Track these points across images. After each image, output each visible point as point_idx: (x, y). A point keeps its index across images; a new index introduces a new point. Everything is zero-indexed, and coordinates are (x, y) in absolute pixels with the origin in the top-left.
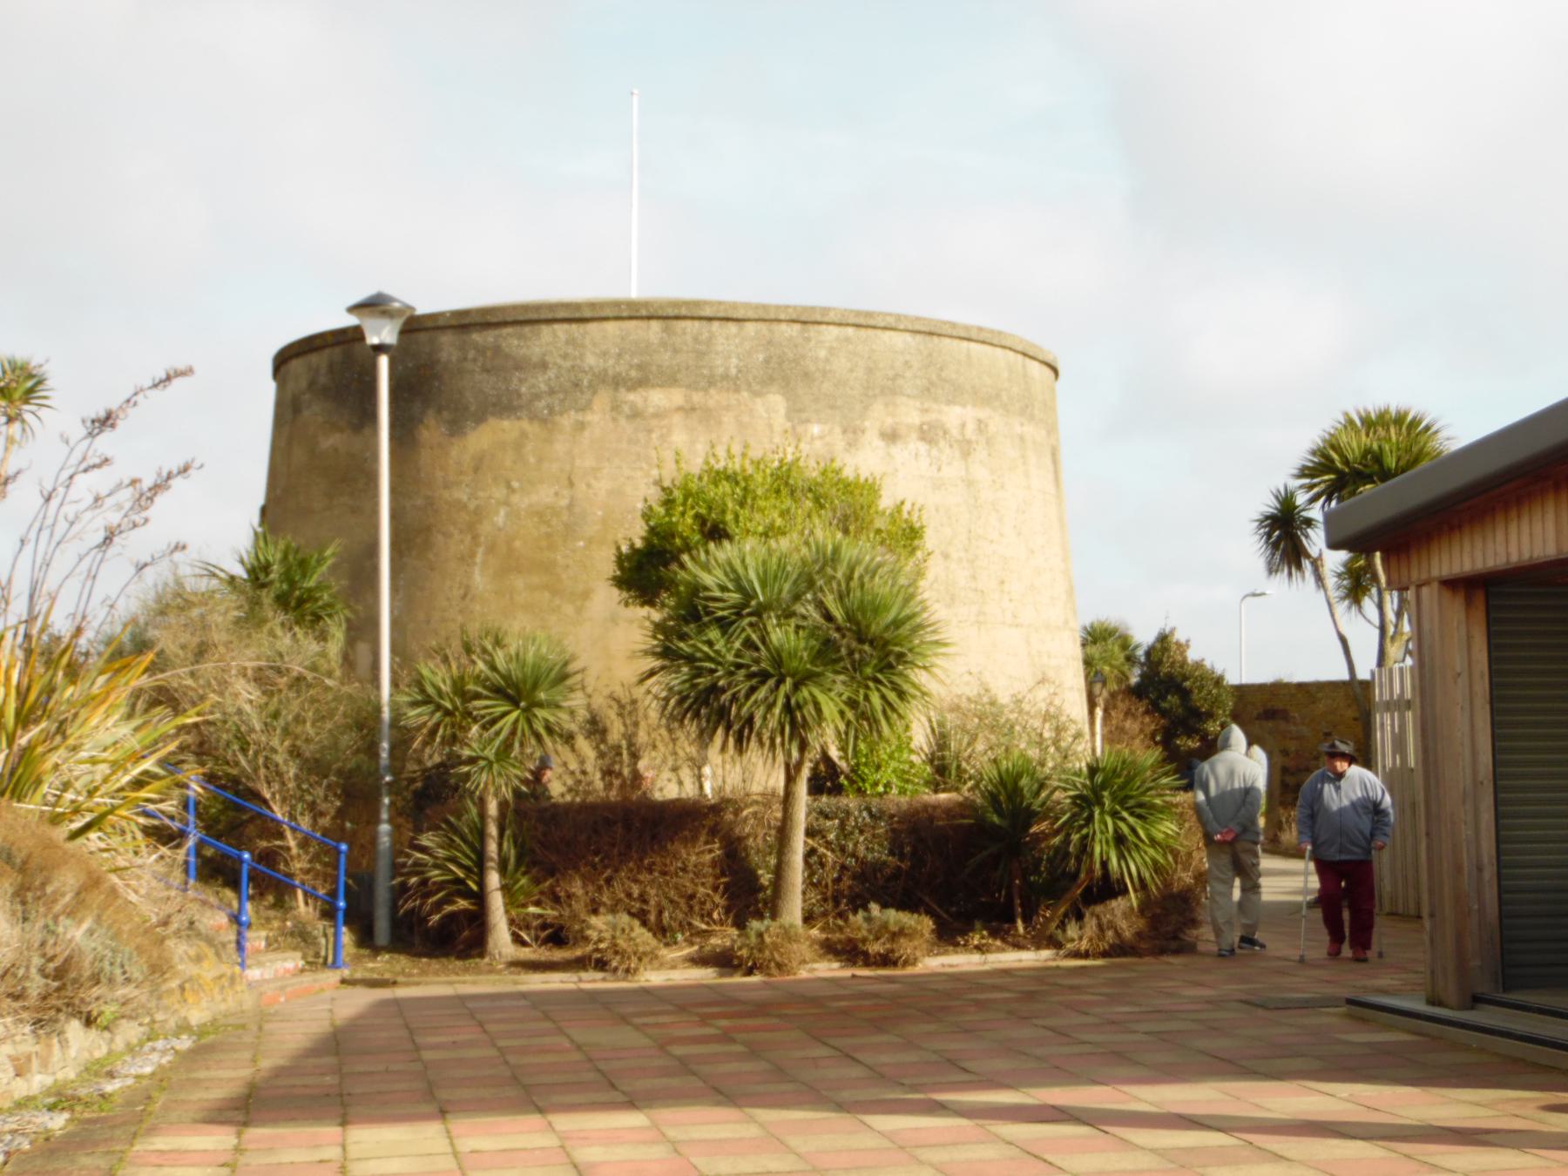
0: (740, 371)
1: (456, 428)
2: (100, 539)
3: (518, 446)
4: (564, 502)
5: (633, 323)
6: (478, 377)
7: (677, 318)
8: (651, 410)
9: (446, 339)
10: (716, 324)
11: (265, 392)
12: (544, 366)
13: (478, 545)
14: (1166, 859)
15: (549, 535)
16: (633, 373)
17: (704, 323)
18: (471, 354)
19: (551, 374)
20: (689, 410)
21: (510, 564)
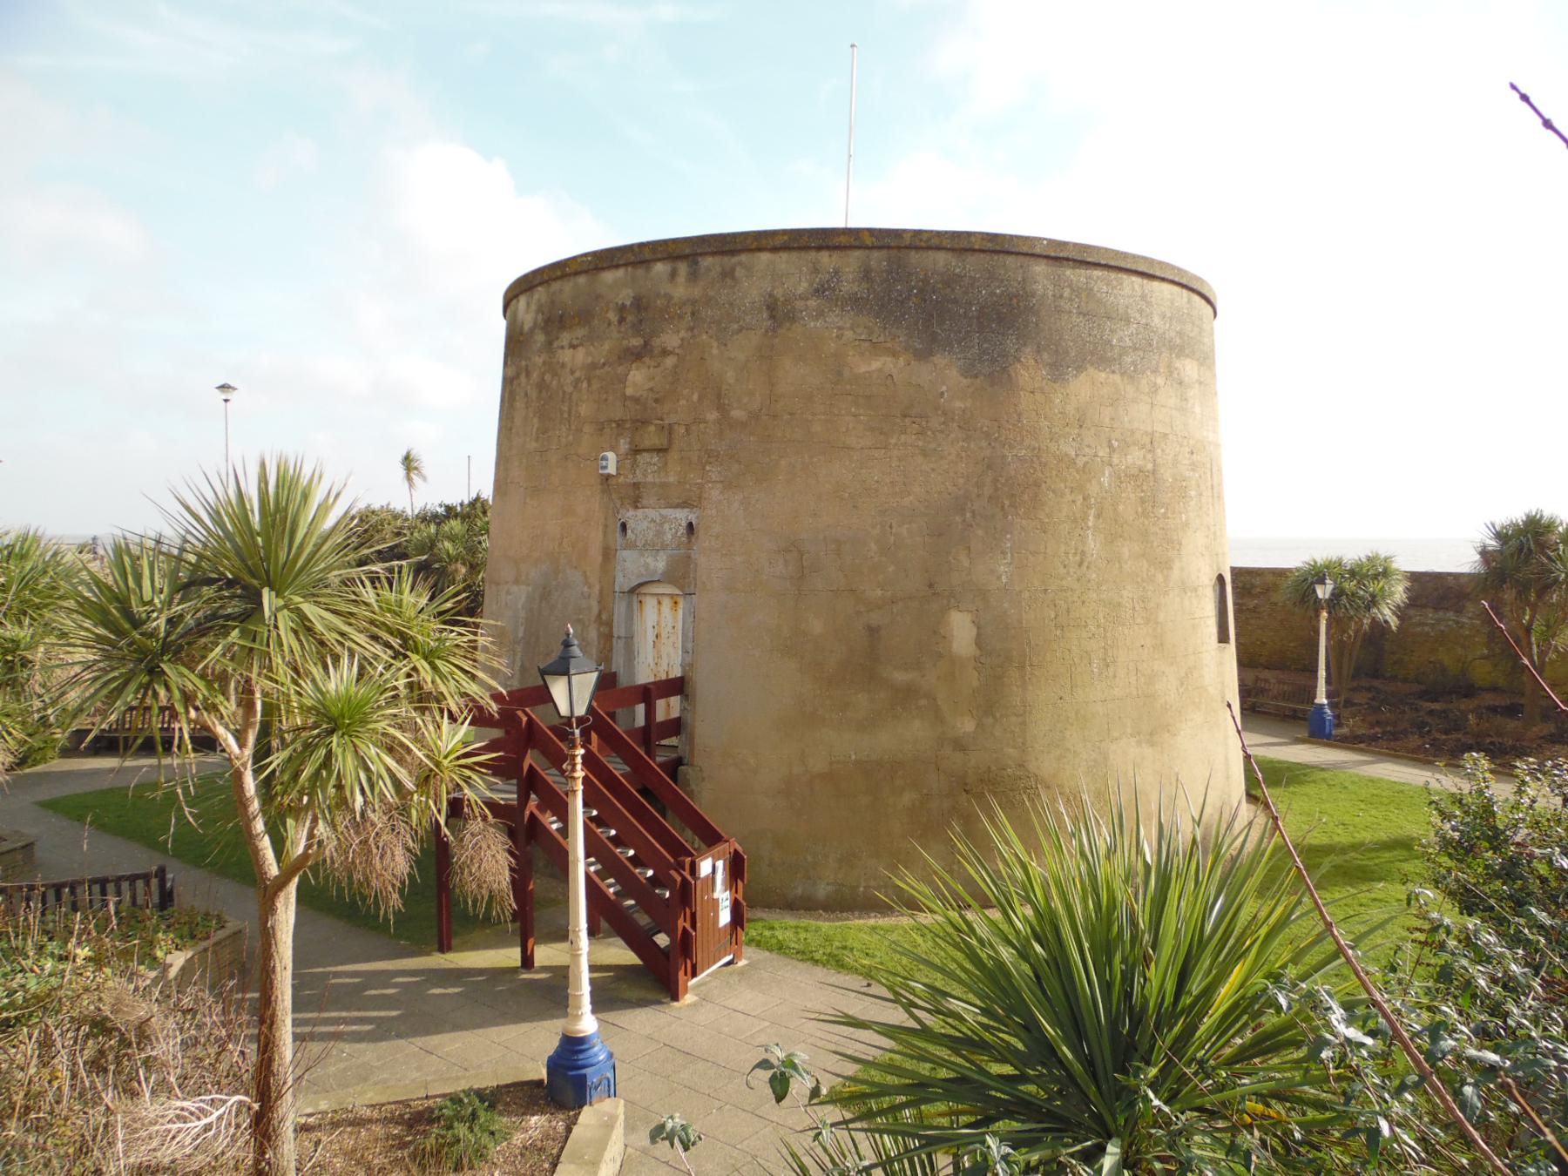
1: (1059, 369)
6: (1076, 319)
9: (1040, 269)
12: (1128, 321)
14: (1037, 1070)
19: (1133, 328)
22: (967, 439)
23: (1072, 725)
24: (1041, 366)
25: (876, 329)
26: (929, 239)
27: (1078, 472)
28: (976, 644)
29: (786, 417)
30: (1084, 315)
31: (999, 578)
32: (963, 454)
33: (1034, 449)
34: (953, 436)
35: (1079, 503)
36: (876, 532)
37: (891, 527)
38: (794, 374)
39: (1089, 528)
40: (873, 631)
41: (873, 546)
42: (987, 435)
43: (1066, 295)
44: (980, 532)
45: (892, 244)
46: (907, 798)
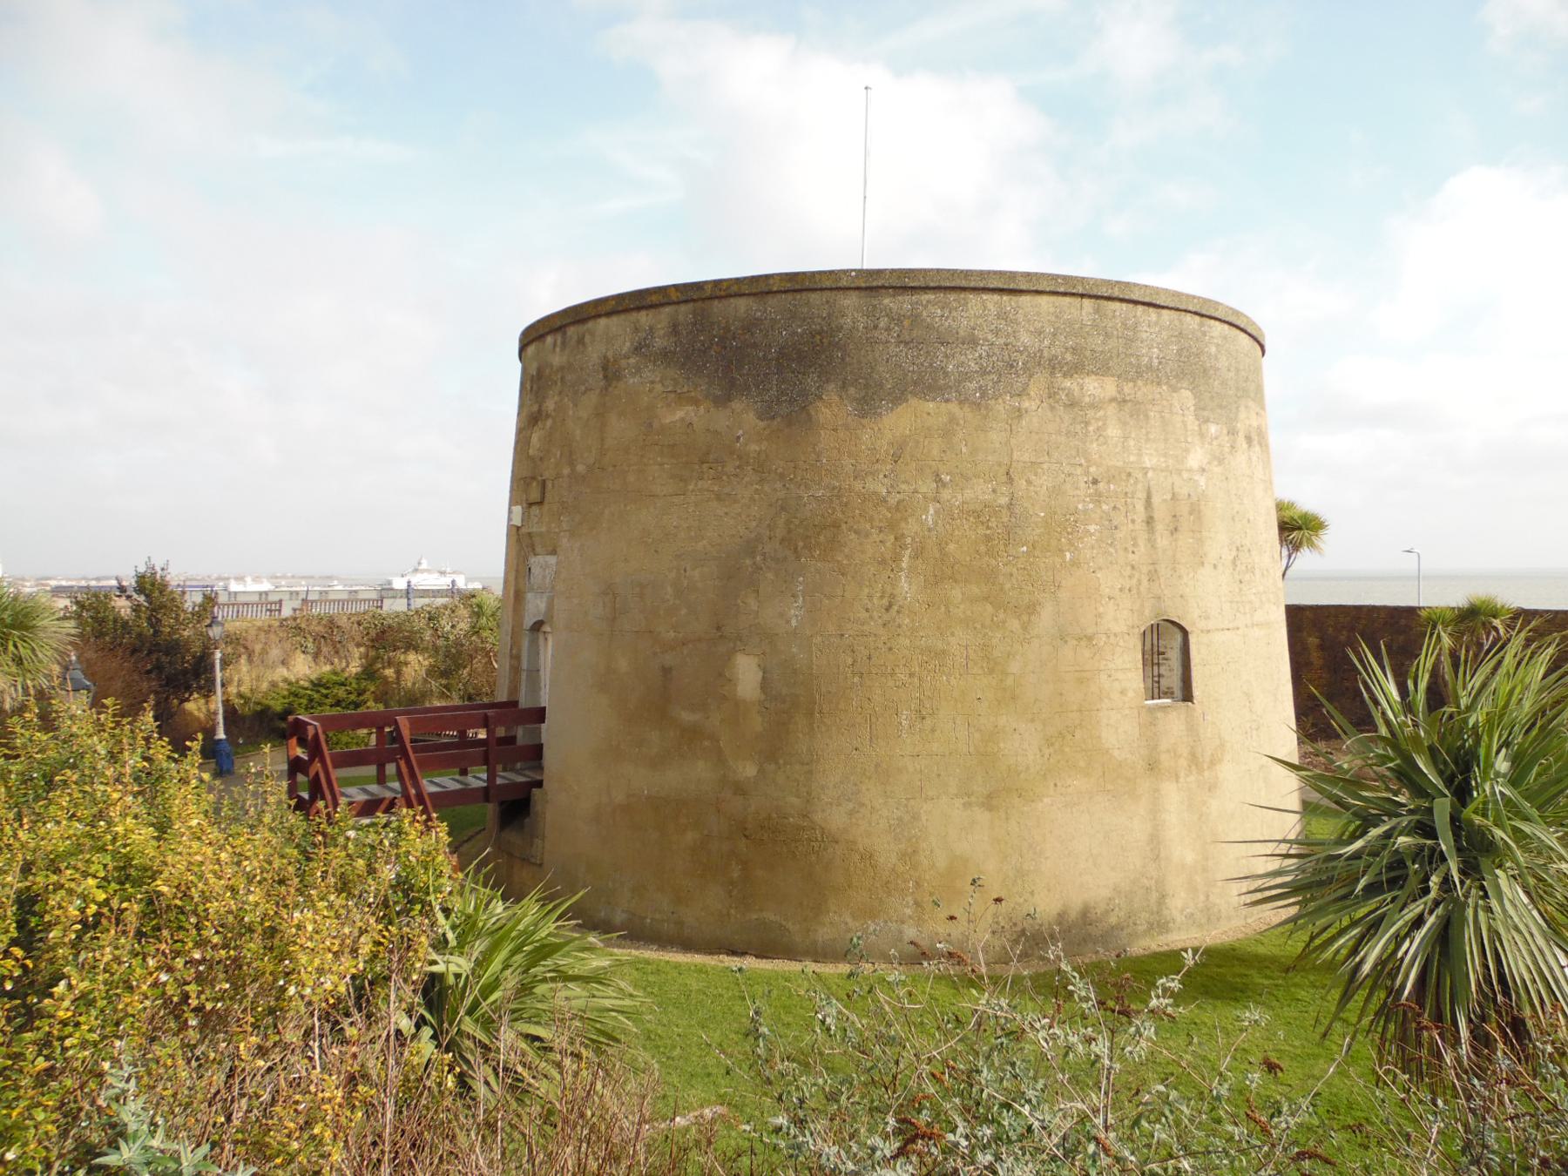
0: (1160, 363)
2: (1011, 470)
3: (947, 434)
4: (1003, 500)
5: (1068, 299)
6: (893, 349)
7: (1109, 298)
8: (1087, 399)
9: (850, 301)
10: (1140, 308)
11: (509, 373)
12: (973, 342)
13: (903, 547)
15: (988, 538)
16: (1069, 357)
17: (1131, 306)
18: (883, 323)
19: (982, 350)
20: (1121, 402)
21: (942, 573)
22: (762, 481)
23: (870, 778)
24: (846, 402)
25: (681, 380)
26: (728, 288)
27: (889, 509)
28: (761, 688)
29: (611, 469)
30: (906, 343)
31: (788, 622)
32: (757, 497)
33: (834, 489)
34: (747, 479)
35: (888, 544)
36: (673, 575)
37: (685, 571)
38: (620, 428)
39: (902, 570)
40: (666, 671)
41: (669, 590)
42: (782, 476)
43: (882, 325)
44: (770, 576)
45: (695, 297)
46: (690, 837)
